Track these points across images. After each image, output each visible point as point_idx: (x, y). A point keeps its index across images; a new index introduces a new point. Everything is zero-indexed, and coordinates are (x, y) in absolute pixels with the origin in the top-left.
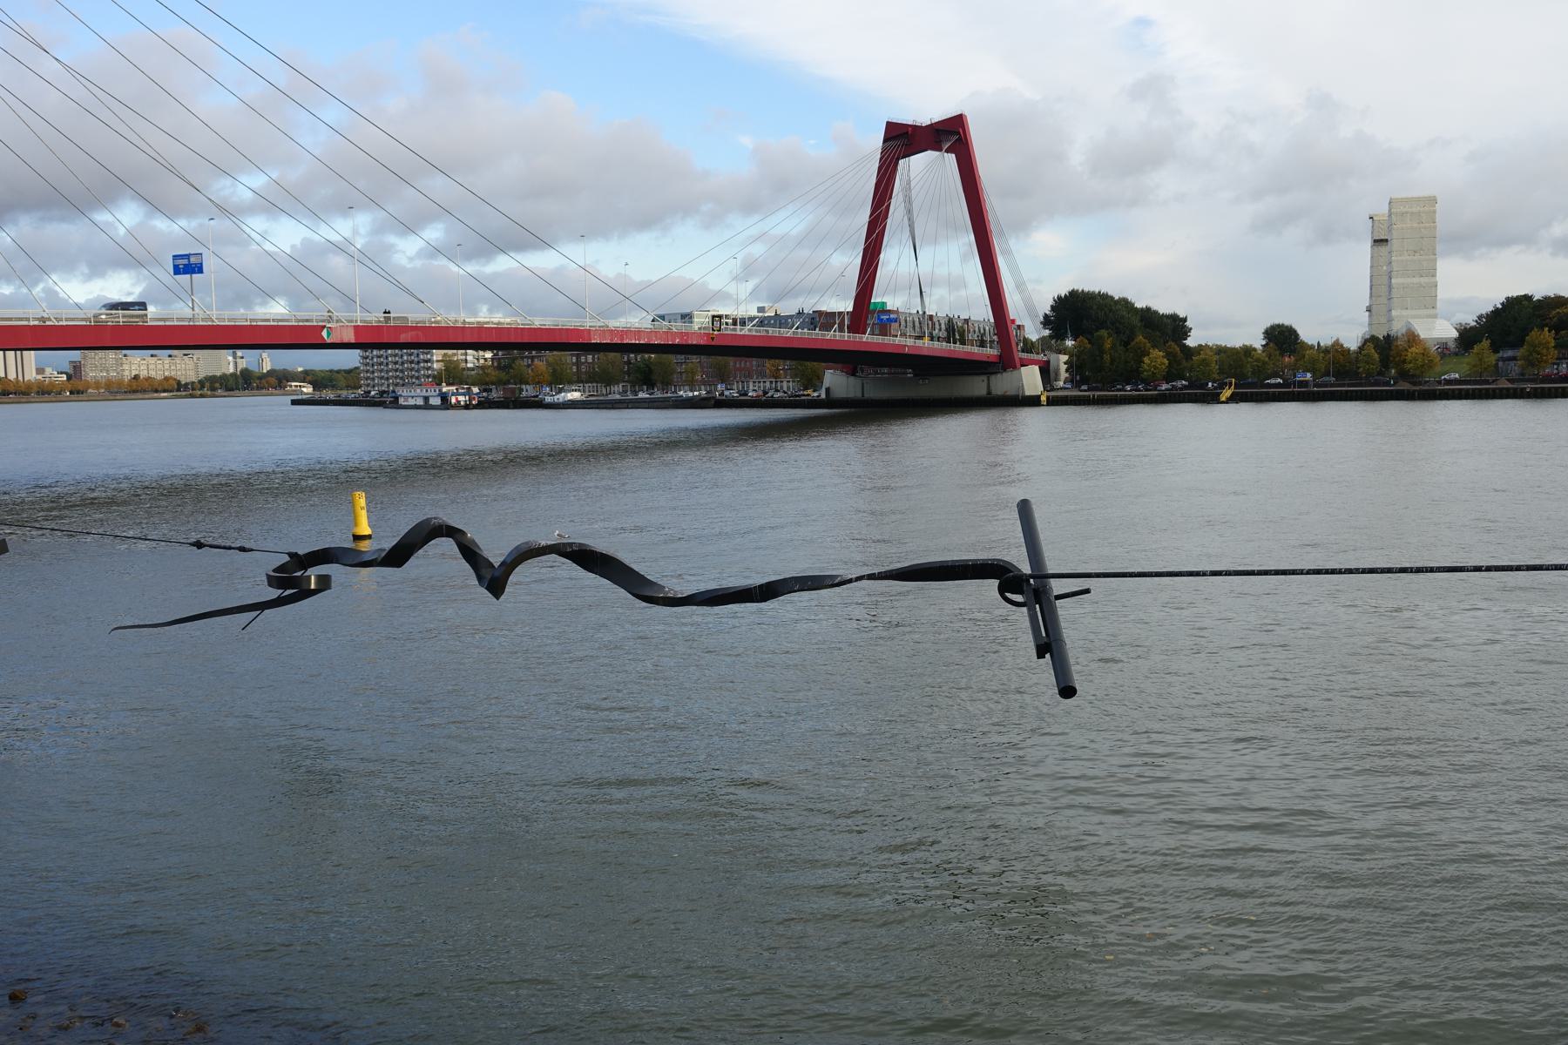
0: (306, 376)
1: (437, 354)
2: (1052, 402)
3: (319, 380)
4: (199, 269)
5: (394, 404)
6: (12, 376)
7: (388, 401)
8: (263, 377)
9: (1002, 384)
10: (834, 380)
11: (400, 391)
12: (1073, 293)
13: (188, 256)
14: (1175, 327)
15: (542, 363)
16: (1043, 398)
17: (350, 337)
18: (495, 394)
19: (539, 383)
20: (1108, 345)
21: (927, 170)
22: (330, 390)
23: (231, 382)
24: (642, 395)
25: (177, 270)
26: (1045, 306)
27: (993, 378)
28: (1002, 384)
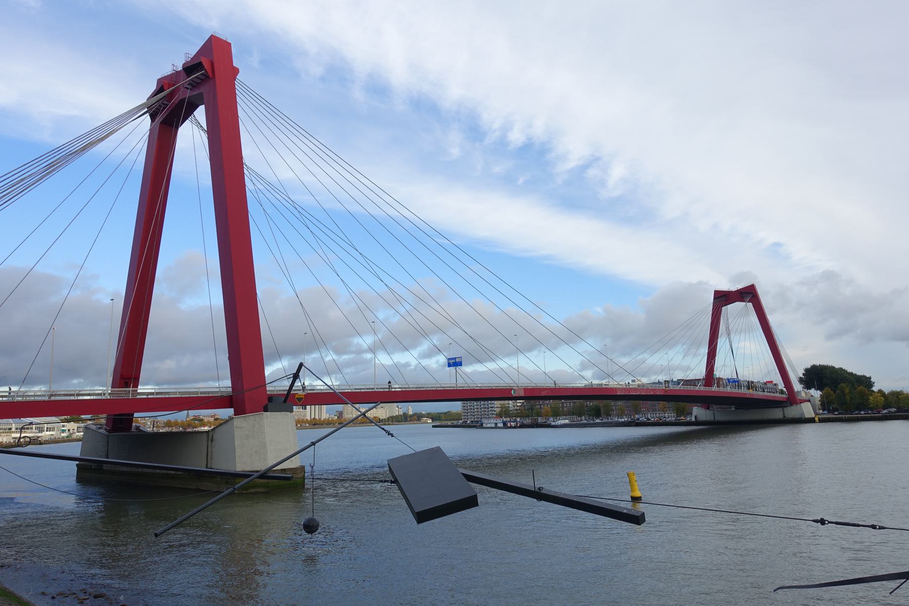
0: (429, 415)
1: (497, 403)
2: (822, 421)
3: (434, 417)
5: (481, 426)
6: (317, 417)
7: (477, 425)
8: (411, 416)
9: (792, 412)
10: (698, 412)
11: (484, 421)
12: (814, 367)
15: (547, 406)
16: (817, 419)
17: (522, 394)
19: (547, 416)
22: (509, 420)
23: (400, 419)
24: (598, 421)
25: (449, 365)
26: (801, 374)
27: (785, 409)
28: (792, 412)
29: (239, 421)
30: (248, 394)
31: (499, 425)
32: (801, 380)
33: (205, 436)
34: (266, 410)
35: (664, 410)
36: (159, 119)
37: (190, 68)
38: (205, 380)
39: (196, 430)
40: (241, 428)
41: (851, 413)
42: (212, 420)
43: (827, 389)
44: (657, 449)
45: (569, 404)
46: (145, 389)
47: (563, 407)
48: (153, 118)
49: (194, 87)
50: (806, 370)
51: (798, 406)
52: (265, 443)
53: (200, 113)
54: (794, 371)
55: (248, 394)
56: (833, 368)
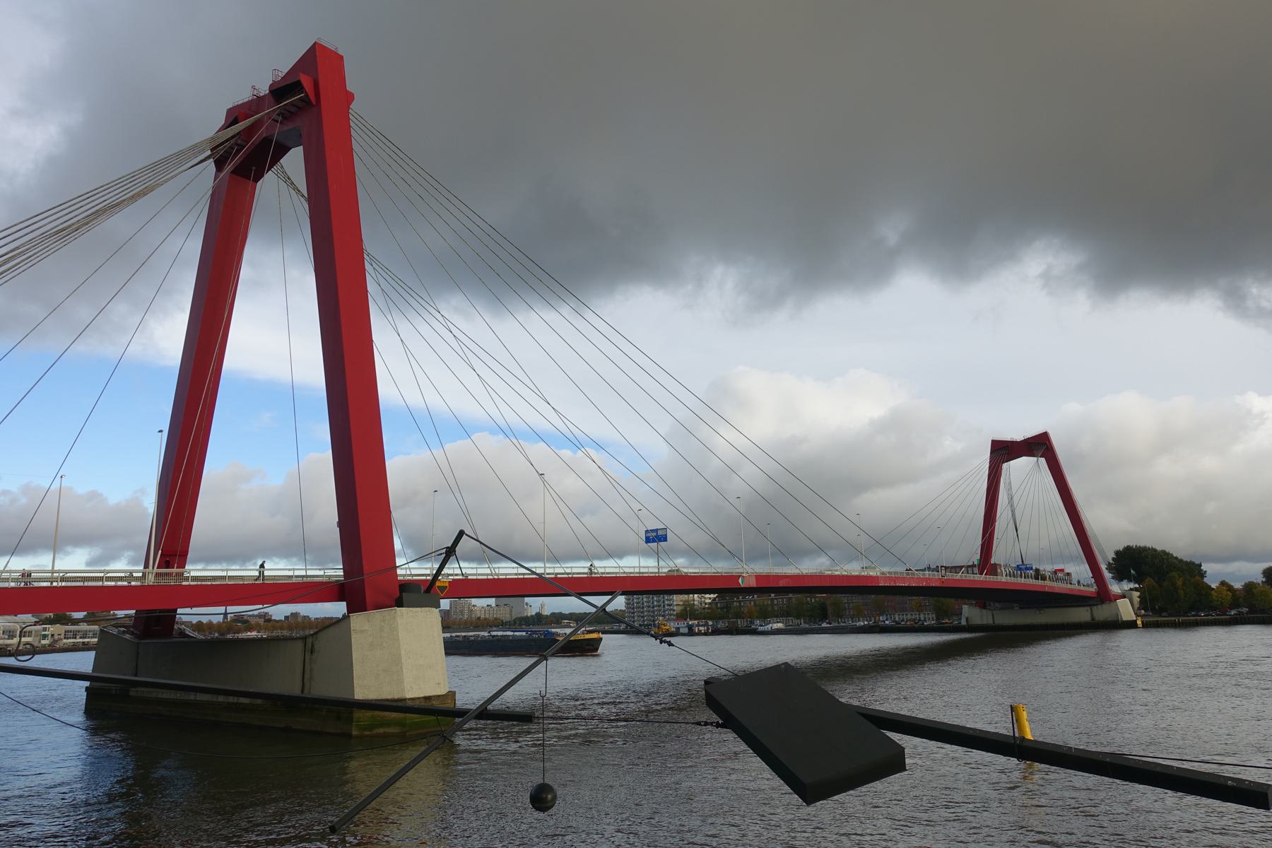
1: (678, 599)
2: (1146, 625)
4: (664, 538)
10: (970, 613)
12: (1128, 549)
13: (657, 530)
14: (1192, 570)
15: (751, 602)
16: (1139, 622)
18: (721, 625)
20: (1180, 583)
21: (1019, 469)
24: (824, 625)
25: (648, 540)
27: (1095, 608)
29: (357, 620)
30: (366, 577)
31: (682, 631)
32: (1110, 568)
33: (300, 644)
34: (400, 603)
35: (920, 609)
36: (228, 168)
37: (281, 91)
38: (620, 554)
39: (241, 636)
40: (362, 632)
41: (1185, 614)
42: (261, 621)
43: (1149, 581)
44: (932, 666)
45: (779, 601)
46: (195, 570)
47: (772, 605)
48: (219, 165)
49: (285, 118)
50: (1117, 553)
51: (1112, 604)
52: (405, 658)
53: (294, 161)
54: (1102, 552)
55: (366, 577)
56: (1155, 550)
